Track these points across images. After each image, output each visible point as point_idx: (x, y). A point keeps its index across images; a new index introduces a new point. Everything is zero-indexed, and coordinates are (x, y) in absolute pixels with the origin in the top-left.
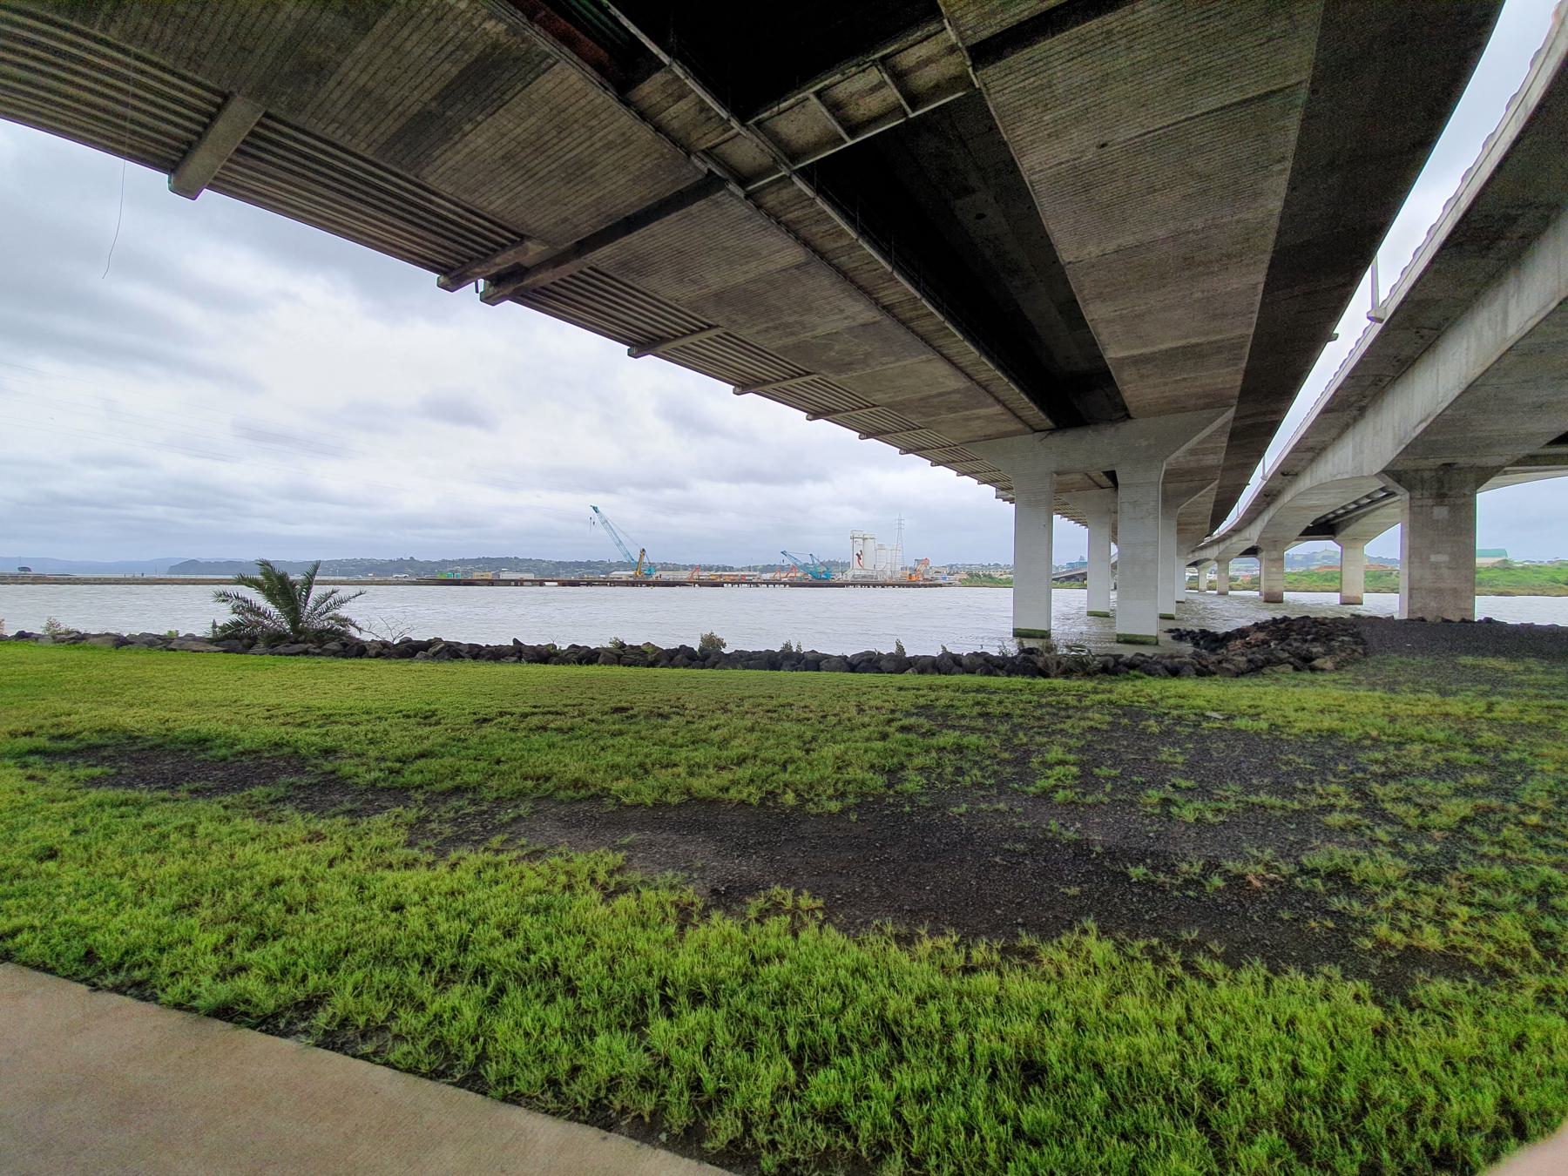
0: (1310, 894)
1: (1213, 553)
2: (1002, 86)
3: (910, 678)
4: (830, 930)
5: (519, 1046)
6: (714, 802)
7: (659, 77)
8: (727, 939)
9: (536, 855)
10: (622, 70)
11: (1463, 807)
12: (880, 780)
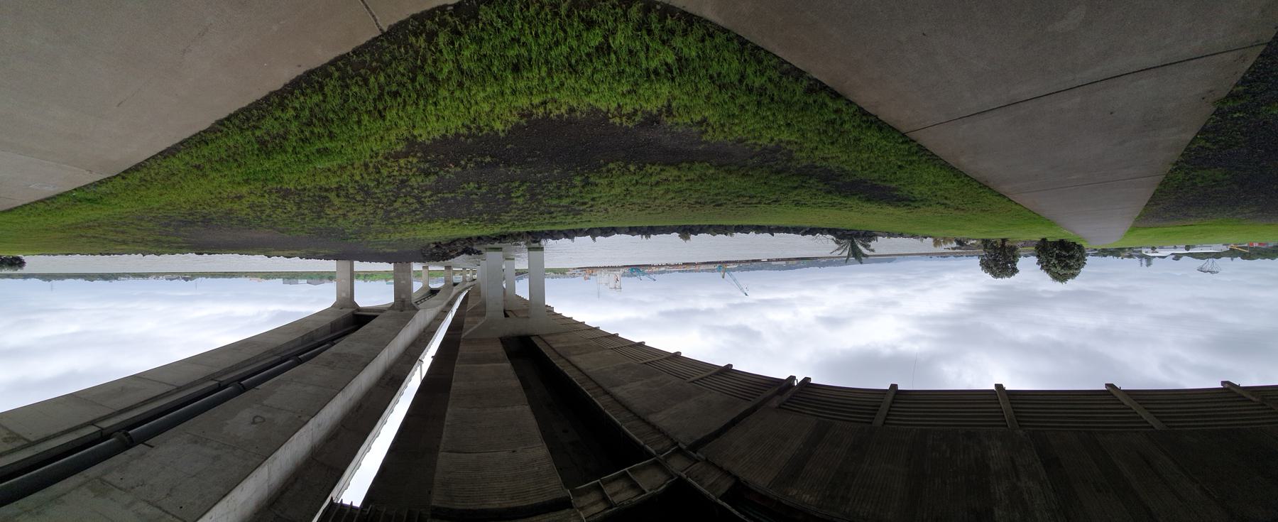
0: (435, 166)
1: (468, 284)
2: (554, 488)
3: (586, 226)
4: (604, 109)
6: (666, 164)
7: (722, 491)
8: (648, 101)
10: (740, 492)
12: (592, 180)
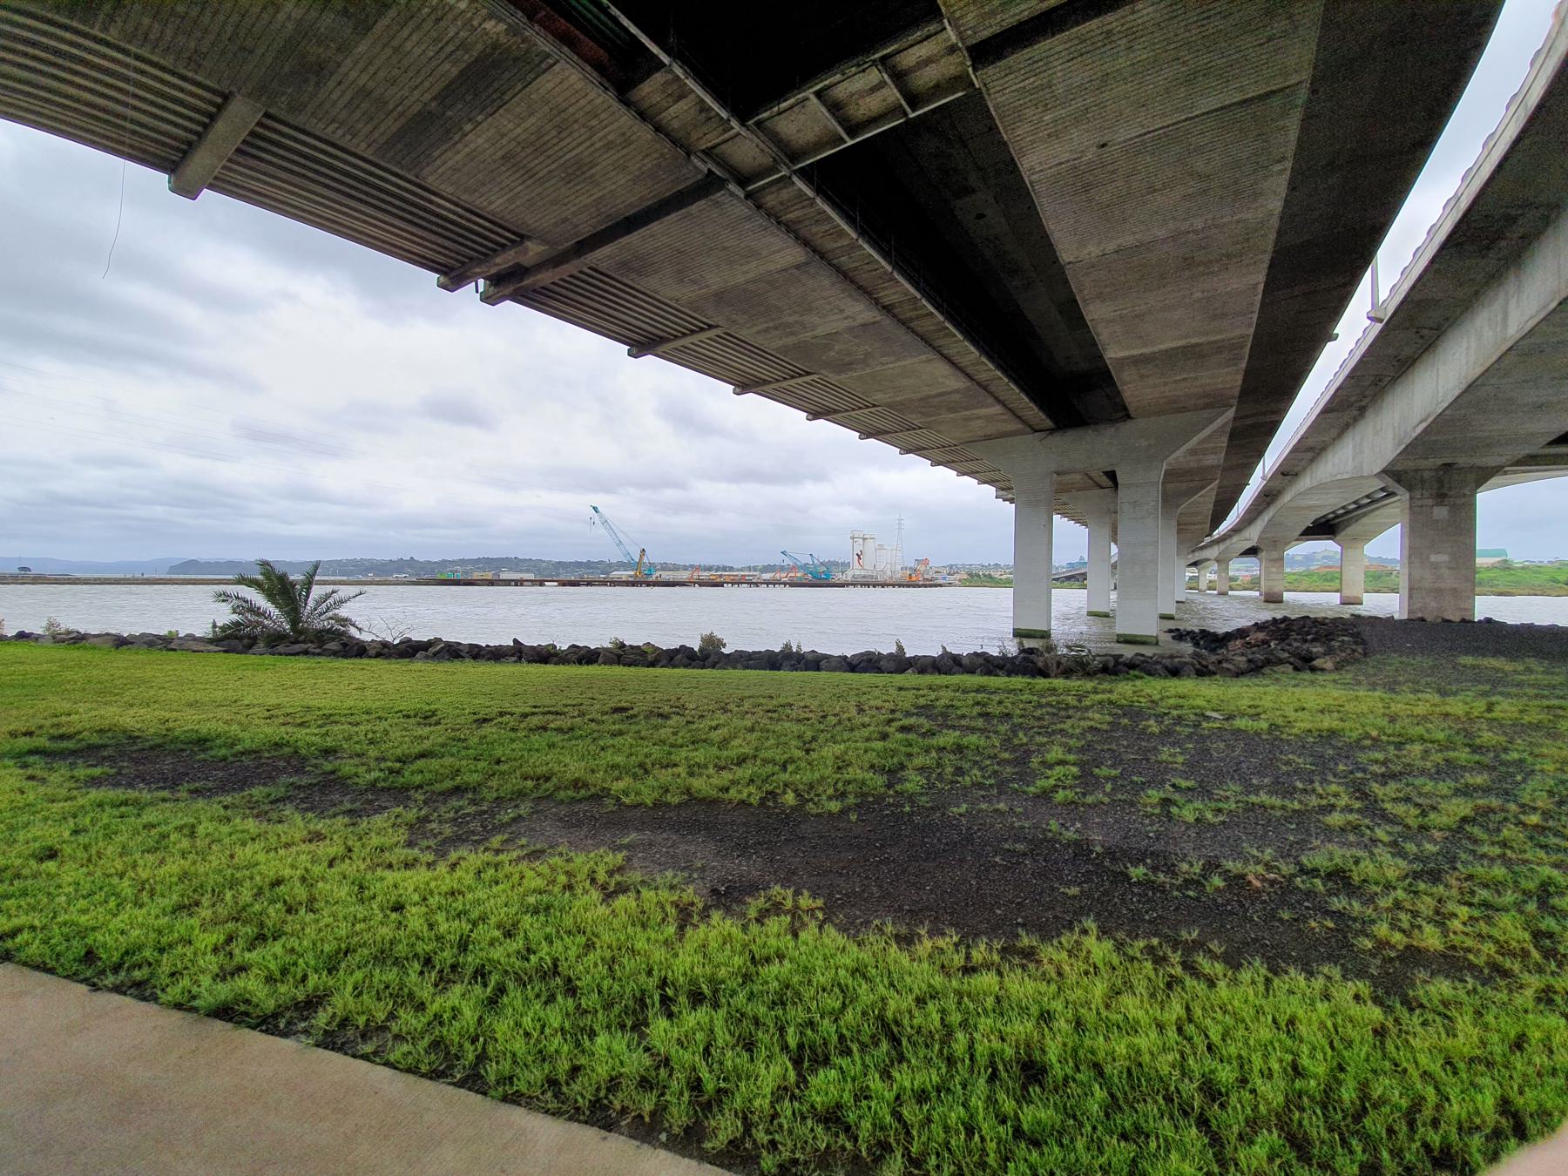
0: (1310, 894)
1: (1213, 553)
2: (1002, 86)
3: (910, 678)
4: (830, 930)
5: (519, 1046)
6: (714, 802)
7: (659, 77)
8: (727, 939)
9: (536, 855)
10: (622, 70)
11: (1463, 807)
12: (880, 780)
